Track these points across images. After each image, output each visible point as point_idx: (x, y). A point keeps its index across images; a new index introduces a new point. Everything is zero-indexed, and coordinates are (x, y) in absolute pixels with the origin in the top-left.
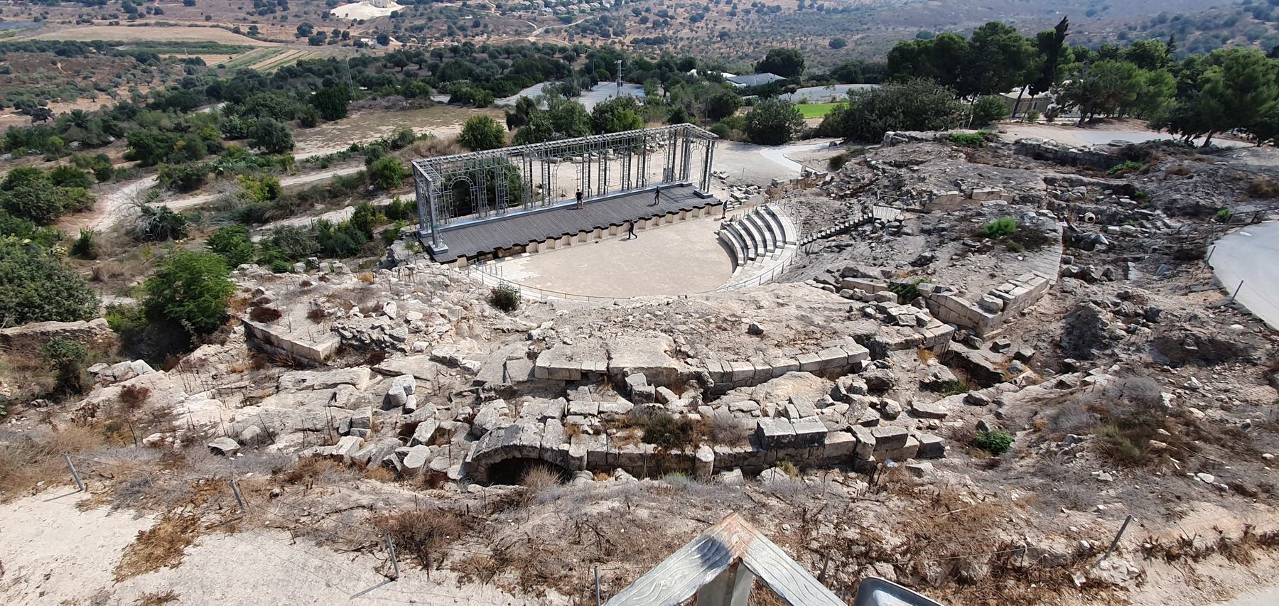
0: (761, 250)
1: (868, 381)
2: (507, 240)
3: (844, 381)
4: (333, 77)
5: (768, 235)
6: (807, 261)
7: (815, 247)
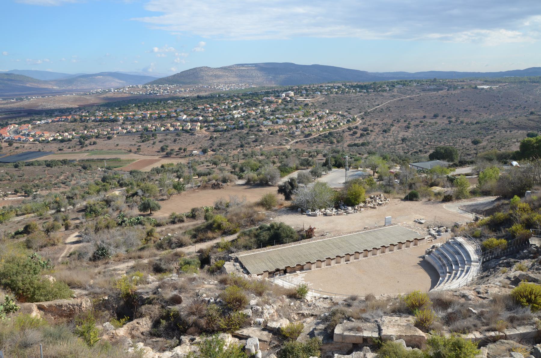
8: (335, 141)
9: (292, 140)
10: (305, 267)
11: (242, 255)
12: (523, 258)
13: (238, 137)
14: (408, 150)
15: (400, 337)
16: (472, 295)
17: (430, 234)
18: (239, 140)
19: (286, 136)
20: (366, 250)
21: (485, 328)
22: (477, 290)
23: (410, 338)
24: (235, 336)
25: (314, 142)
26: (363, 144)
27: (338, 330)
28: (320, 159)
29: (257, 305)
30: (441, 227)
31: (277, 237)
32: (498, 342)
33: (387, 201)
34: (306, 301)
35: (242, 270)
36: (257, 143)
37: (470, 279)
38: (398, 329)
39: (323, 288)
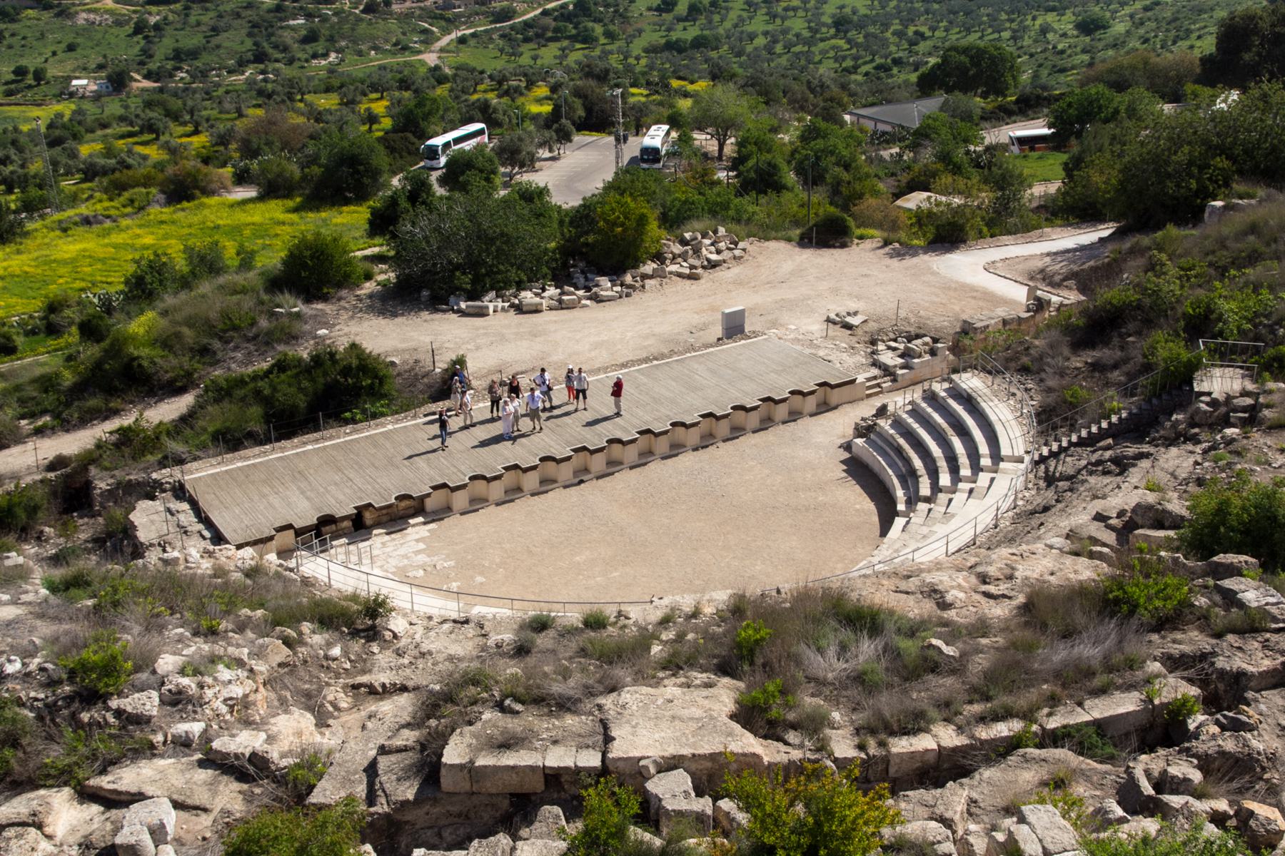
0: (945, 479)
1: (1205, 763)
2: (383, 491)
3: (1145, 766)
4: (623, 621)
5: (957, 444)
6: (1050, 494)
7: (1068, 465)
8: (598, 29)
9: (446, 31)
10: (430, 504)
11: (201, 473)
12: (1170, 442)
13: (243, 22)
14: (856, 58)
15: (669, 765)
16: (959, 587)
17: (875, 364)
18: (250, 35)
19: (421, 18)
20: (648, 431)
21: (977, 708)
22: (980, 569)
23: (709, 764)
24: (87, 795)
25: (527, 40)
26: (699, 43)
27: (453, 754)
28: (537, 105)
29: (182, 672)
30: (918, 336)
31: (347, 391)
32: (1012, 759)
33: (737, 253)
34: (388, 635)
35: (201, 527)
36: (319, 47)
37: (987, 519)
38: (669, 733)
39: (434, 590)
